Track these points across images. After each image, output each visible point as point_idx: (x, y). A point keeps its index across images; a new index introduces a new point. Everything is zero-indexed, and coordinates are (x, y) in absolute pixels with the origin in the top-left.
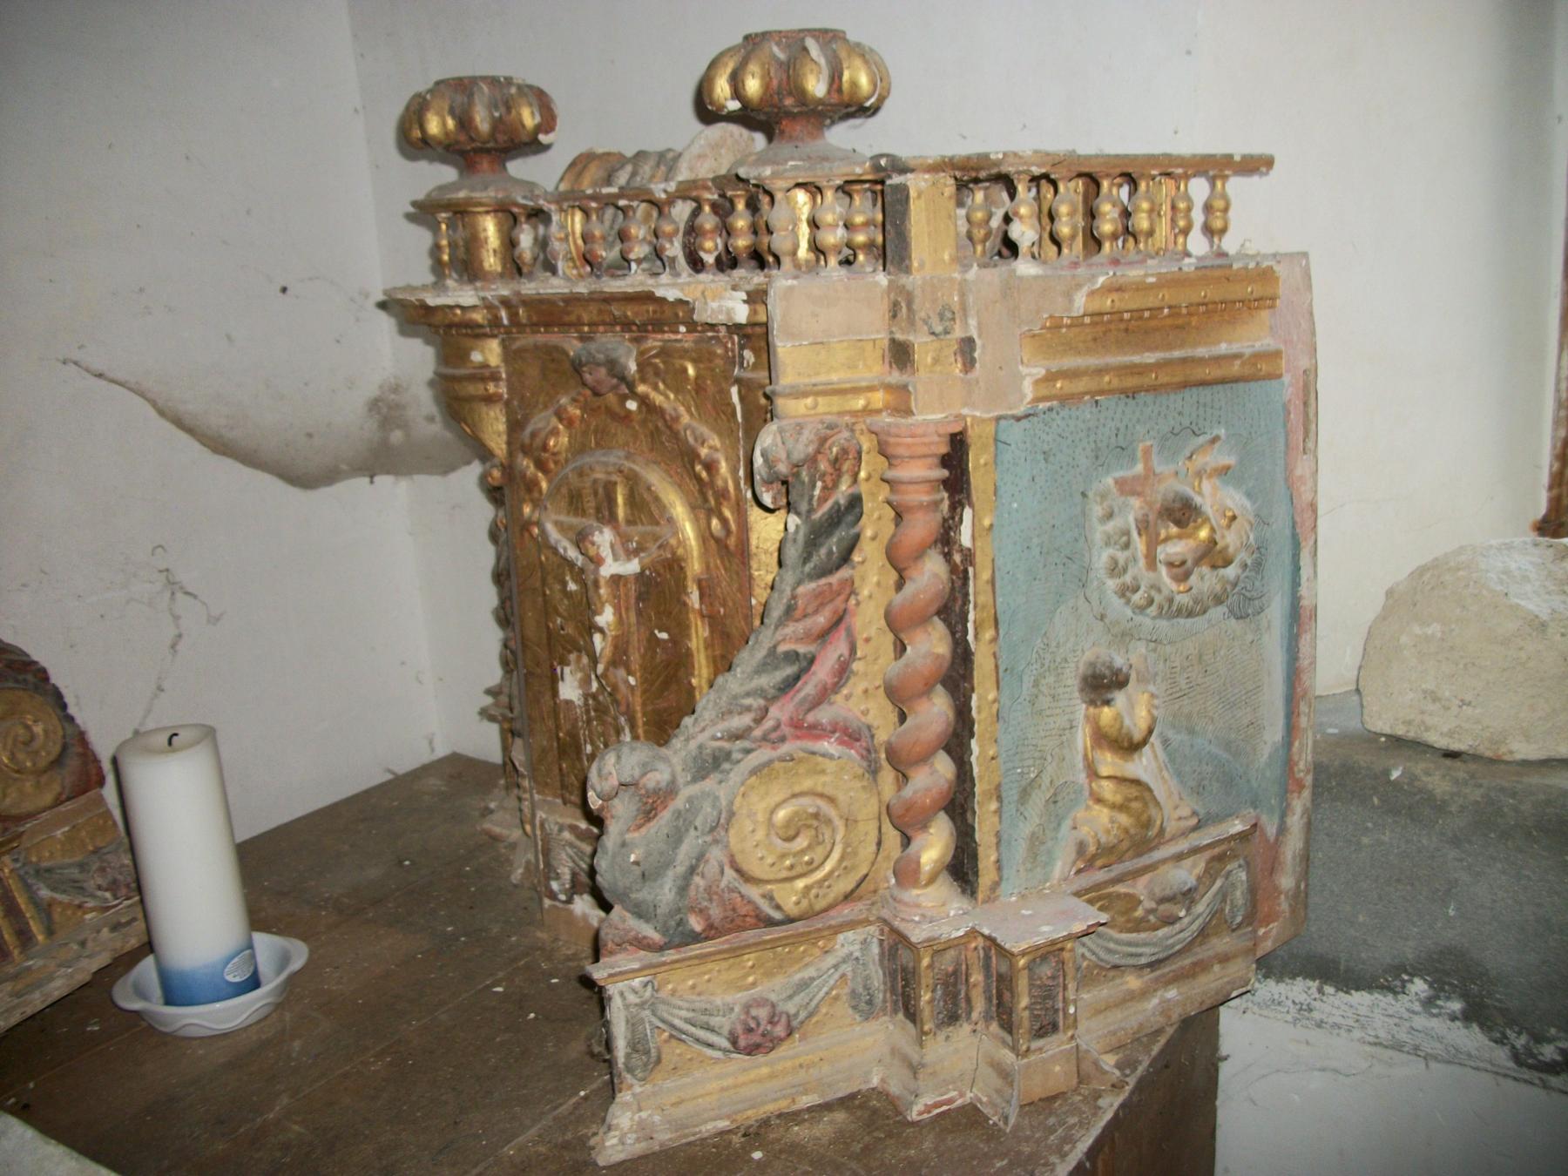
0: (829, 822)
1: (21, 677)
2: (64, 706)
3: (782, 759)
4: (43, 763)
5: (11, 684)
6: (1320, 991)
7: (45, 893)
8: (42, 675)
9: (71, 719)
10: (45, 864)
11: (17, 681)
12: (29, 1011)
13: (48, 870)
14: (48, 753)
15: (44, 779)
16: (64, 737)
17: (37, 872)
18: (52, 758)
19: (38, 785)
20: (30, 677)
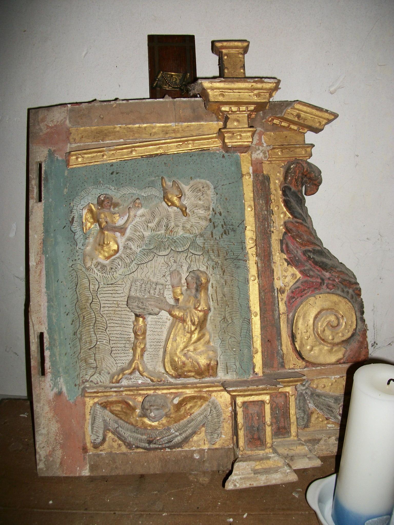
0: (176, 377)
1: (346, 290)
2: (363, 313)
3: (169, 393)
4: (337, 340)
5: (339, 292)
6: (184, 342)
7: (311, 406)
8: (358, 292)
9: (363, 321)
10: (318, 391)
11: (343, 291)
12: (255, 484)
13: (319, 396)
14: (343, 336)
15: (335, 348)
16: (355, 330)
17: (312, 394)
18: (344, 338)
19: (330, 351)
20: (351, 291)
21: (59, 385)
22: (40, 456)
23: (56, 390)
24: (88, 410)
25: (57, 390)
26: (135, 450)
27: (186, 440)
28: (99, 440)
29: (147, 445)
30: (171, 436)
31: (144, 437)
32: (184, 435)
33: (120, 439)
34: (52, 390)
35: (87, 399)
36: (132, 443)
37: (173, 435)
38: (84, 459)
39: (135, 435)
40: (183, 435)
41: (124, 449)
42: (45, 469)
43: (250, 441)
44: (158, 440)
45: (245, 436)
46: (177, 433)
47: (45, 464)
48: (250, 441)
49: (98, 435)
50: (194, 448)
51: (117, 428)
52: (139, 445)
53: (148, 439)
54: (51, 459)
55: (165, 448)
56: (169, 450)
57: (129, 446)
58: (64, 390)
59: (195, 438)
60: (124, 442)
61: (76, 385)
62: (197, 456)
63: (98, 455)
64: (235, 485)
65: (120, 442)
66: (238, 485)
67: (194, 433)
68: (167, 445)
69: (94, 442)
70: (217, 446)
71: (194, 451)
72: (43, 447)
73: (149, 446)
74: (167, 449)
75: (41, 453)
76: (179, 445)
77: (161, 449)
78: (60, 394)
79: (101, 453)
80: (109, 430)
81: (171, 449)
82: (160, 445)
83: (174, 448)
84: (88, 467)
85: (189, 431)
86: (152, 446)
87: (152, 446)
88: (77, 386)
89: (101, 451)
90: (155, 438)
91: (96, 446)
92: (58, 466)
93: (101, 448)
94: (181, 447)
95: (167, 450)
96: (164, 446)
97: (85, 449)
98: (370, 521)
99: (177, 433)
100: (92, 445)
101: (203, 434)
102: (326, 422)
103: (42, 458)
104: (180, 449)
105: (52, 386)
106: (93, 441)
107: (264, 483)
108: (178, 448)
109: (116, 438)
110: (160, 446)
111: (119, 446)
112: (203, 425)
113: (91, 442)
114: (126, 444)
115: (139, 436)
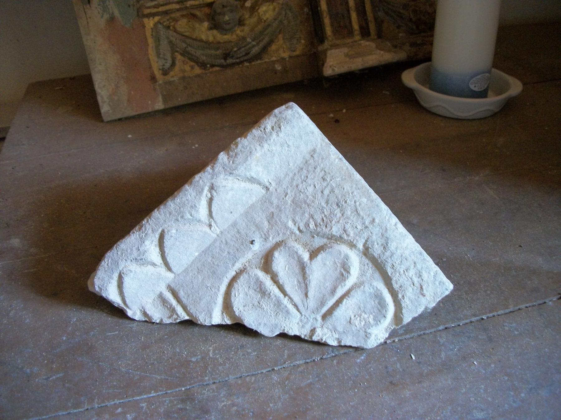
21: (109, 9)
22: (102, 97)
23: (106, 16)
24: (148, 33)
25: (108, 15)
26: (211, 70)
27: (265, 49)
28: (168, 65)
29: (223, 61)
30: (248, 47)
31: (219, 52)
32: (261, 45)
33: (190, 59)
34: (102, 17)
35: (146, 20)
36: (206, 61)
37: (250, 45)
38: (155, 89)
39: (209, 52)
40: (261, 45)
41: (198, 70)
42: (111, 111)
43: (337, 31)
44: (235, 51)
45: (332, 25)
46: (254, 43)
47: (110, 105)
48: (337, 31)
49: (166, 58)
50: (274, 59)
51: (186, 48)
52: (214, 63)
53: (224, 52)
54: (116, 98)
55: (242, 62)
56: (248, 64)
57: (203, 65)
58: (117, 14)
59: (274, 47)
60: (197, 63)
61: (129, 6)
62: (278, 67)
63: (170, 83)
64: (333, 70)
65: (192, 64)
66: (336, 69)
67: (271, 42)
68: (245, 58)
69: (163, 69)
70: (298, 53)
71: (274, 62)
72: (104, 86)
73: (225, 61)
74: (245, 63)
75: (102, 93)
76: (258, 56)
77: (238, 64)
78: (112, 19)
79: (172, 79)
80: (177, 52)
81: (250, 62)
82: (237, 58)
83: (253, 61)
84: (160, 98)
85: (266, 40)
86: (229, 61)
87: (229, 61)
88: (132, 7)
89: (172, 77)
90: (232, 49)
91: (165, 73)
92: (125, 104)
93: (172, 73)
94: (261, 59)
95: (247, 64)
96: (242, 59)
97: (153, 79)
98: (474, 79)
99: (254, 43)
100: (161, 72)
101: (281, 42)
102: (397, 31)
103: (106, 99)
104: (259, 62)
105: (101, 12)
106: (161, 68)
107: (362, 65)
108: (257, 60)
109: (187, 60)
110: (238, 61)
111: (192, 67)
112: (280, 33)
113: (160, 69)
114: (199, 64)
115: (213, 52)
